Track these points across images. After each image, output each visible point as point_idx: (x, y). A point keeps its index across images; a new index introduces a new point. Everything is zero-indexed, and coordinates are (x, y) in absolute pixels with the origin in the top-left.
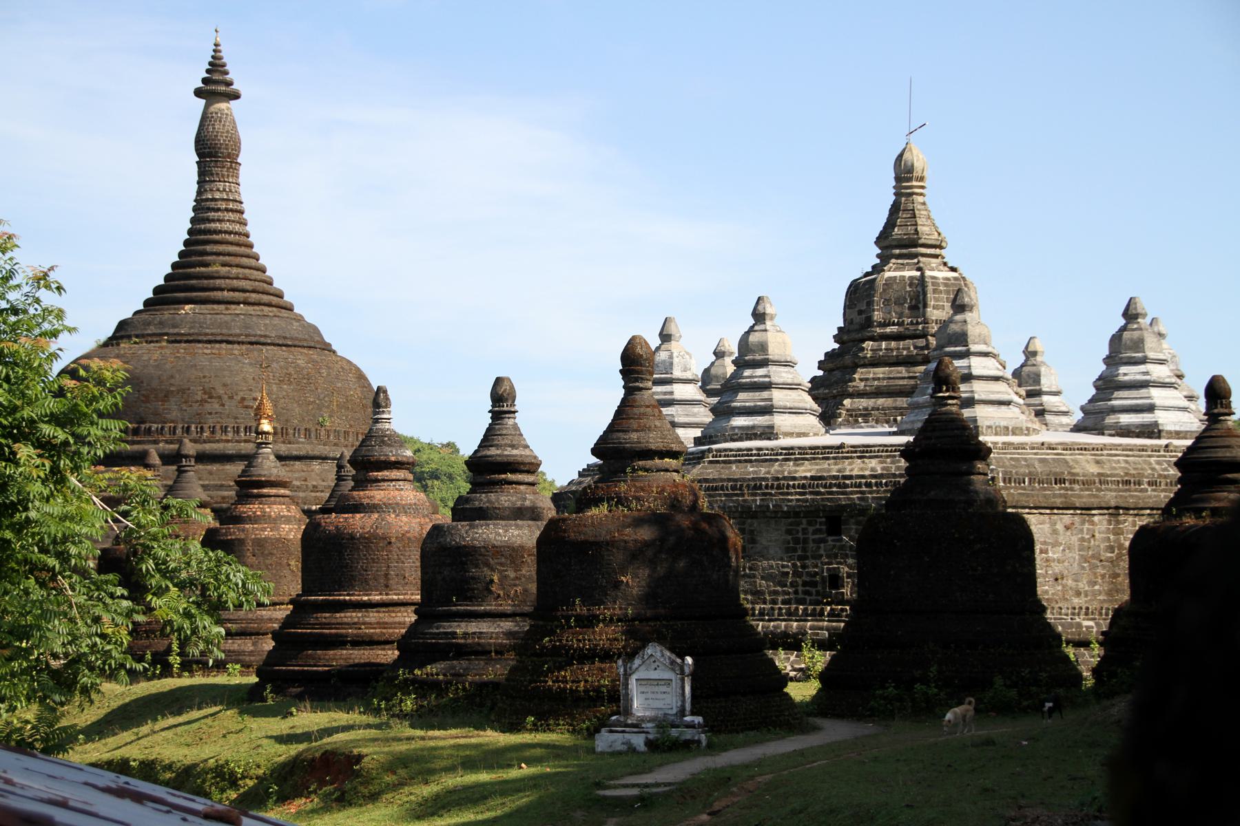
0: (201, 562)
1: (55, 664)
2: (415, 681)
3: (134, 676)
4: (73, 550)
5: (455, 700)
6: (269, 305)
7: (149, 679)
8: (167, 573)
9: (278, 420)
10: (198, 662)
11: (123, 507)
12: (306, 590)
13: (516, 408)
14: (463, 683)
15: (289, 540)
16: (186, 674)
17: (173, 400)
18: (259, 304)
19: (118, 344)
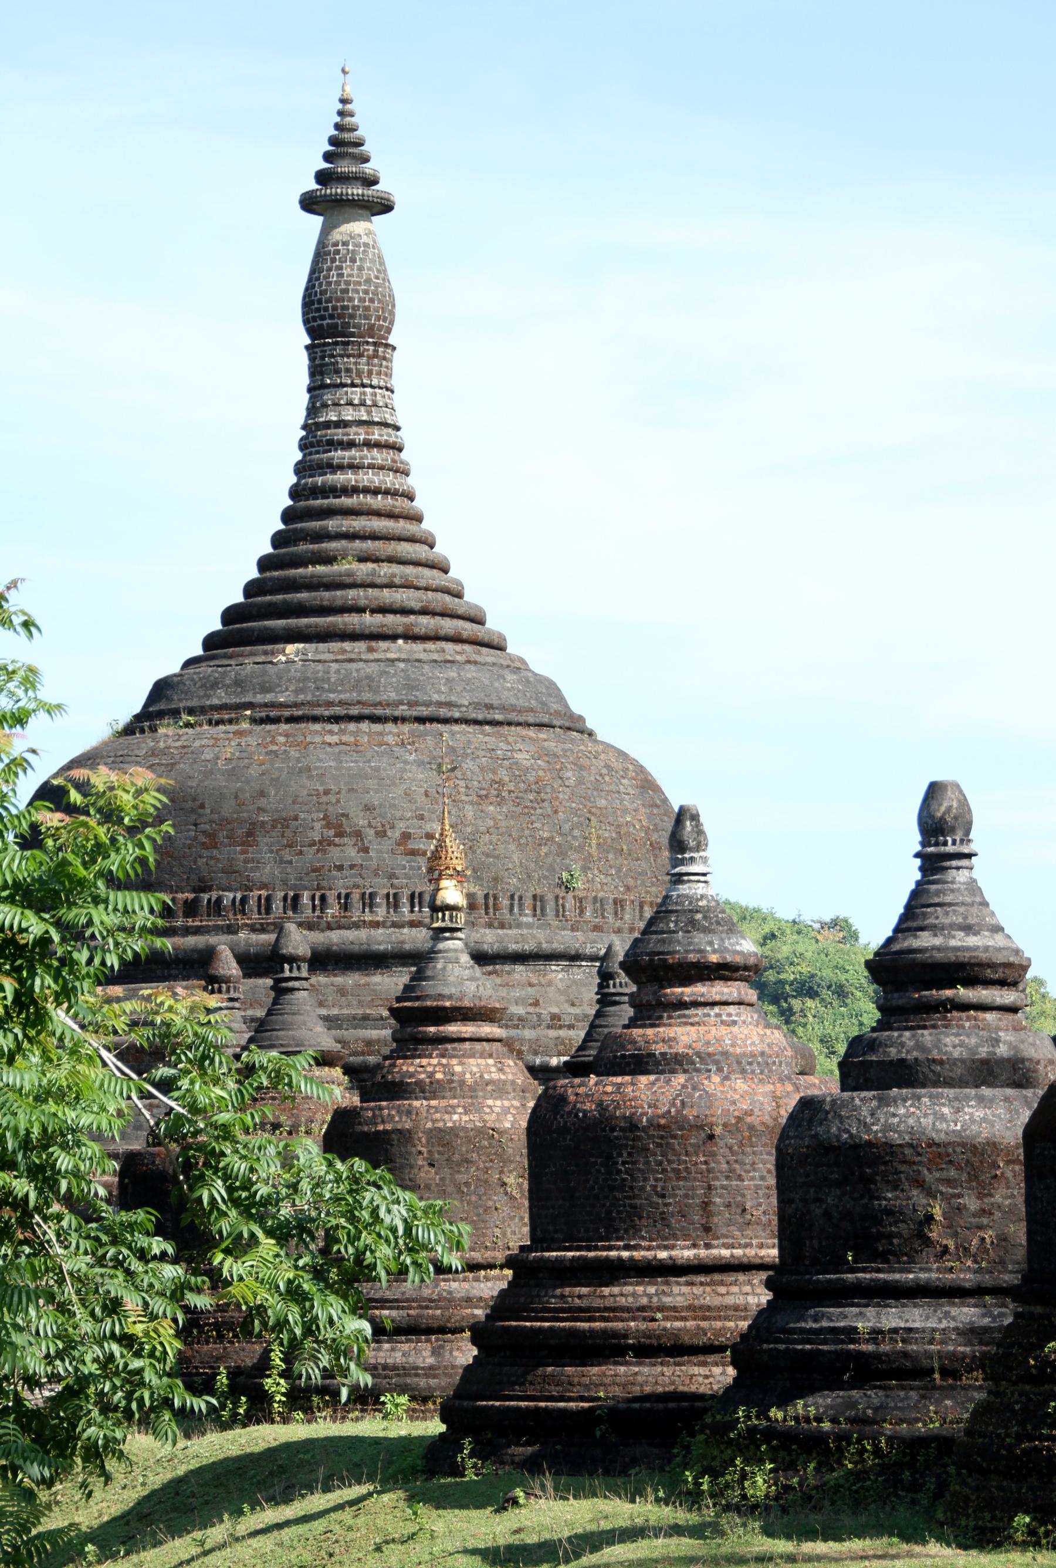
0: (319, 1183)
1: (35, 1399)
2: (771, 1433)
3: (190, 1422)
4: (64, 1162)
5: (858, 1475)
6: (457, 639)
7: (225, 1427)
8: (252, 1208)
9: (478, 879)
10: (322, 1391)
11: (163, 1071)
12: (540, 1237)
13: (973, 847)
14: (875, 1439)
15: (501, 1133)
16: (299, 1415)
17: (263, 840)
18: (436, 638)
19: (154, 729)
